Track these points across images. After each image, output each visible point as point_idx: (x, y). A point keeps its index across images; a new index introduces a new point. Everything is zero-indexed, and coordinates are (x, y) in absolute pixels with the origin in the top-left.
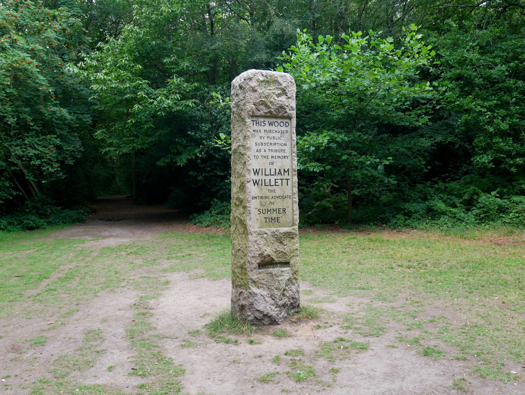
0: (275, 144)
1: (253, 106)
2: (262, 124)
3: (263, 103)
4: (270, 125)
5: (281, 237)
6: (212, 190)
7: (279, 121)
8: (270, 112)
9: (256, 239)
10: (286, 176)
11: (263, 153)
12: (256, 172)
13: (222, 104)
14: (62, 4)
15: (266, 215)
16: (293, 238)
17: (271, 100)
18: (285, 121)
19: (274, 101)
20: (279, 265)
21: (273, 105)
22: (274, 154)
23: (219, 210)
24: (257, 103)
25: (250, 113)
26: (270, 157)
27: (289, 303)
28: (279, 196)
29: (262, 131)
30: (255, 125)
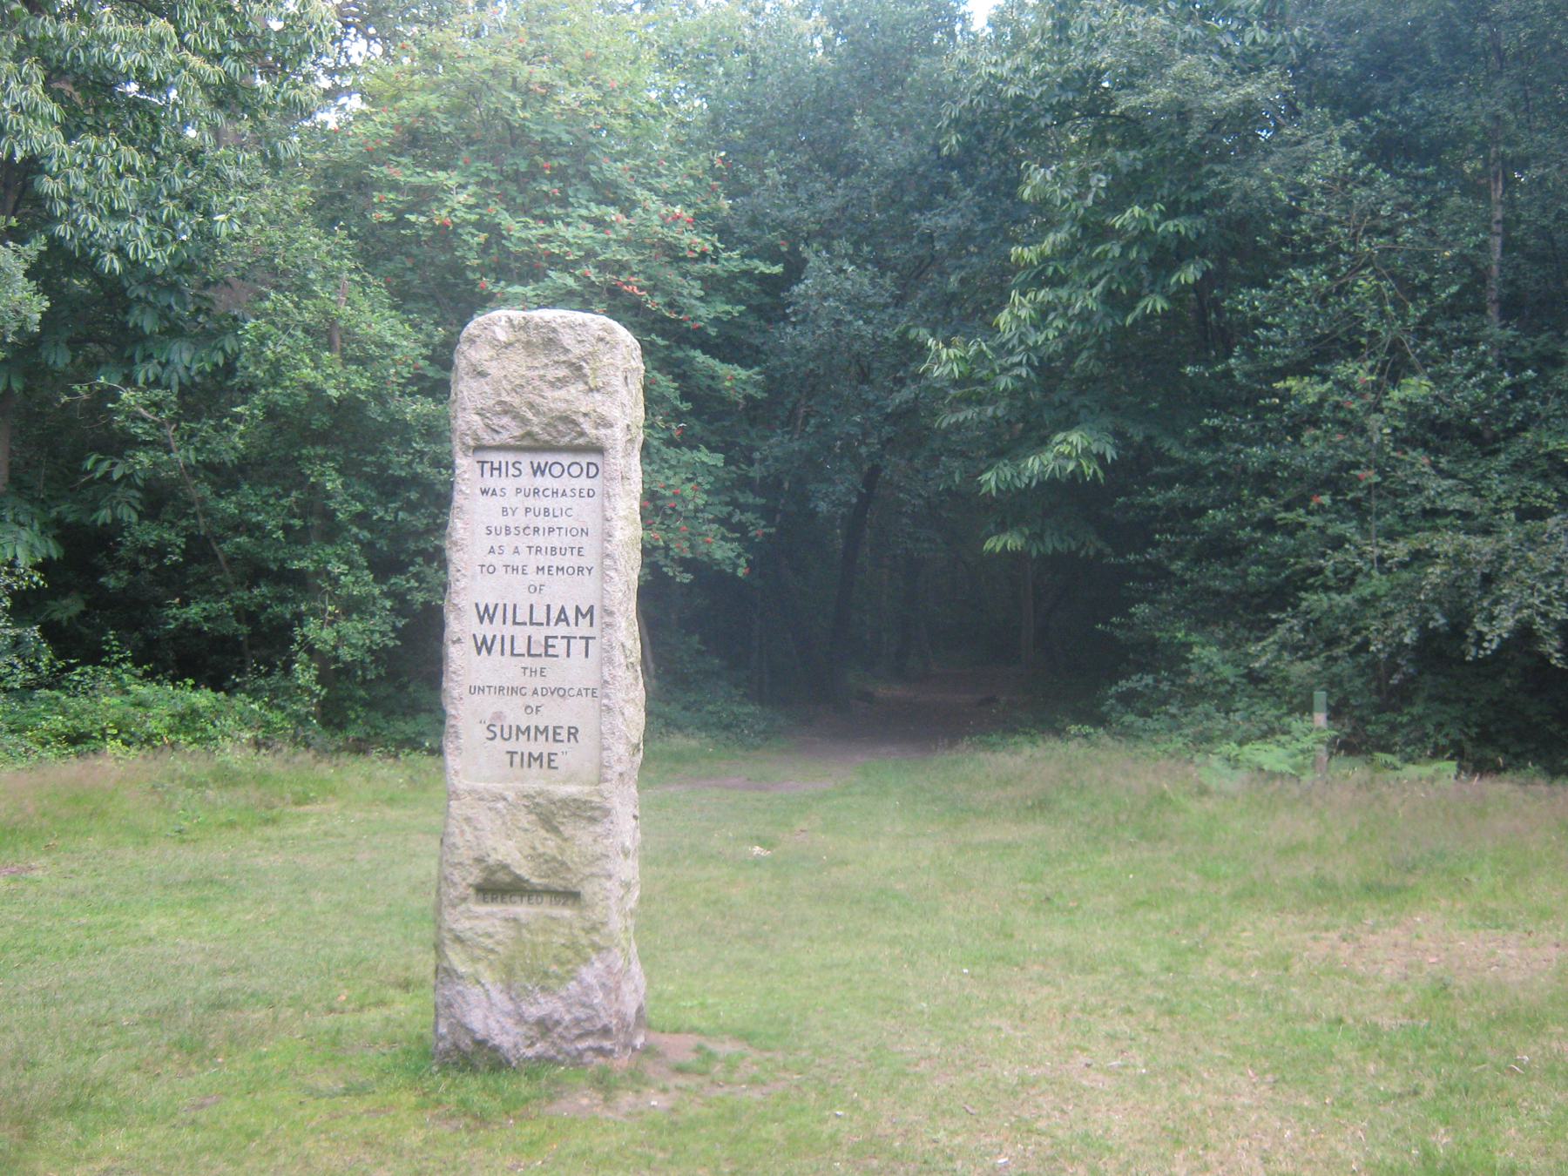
0: (551, 530)
1: (477, 418)
2: (512, 471)
3: (507, 410)
4: (535, 474)
7: (566, 459)
8: (529, 434)
10: (584, 628)
11: (508, 558)
12: (486, 614)
15: (510, 746)
18: (584, 460)
20: (546, 899)
22: (544, 560)
26: (531, 569)
27: (567, 1017)
29: (510, 491)
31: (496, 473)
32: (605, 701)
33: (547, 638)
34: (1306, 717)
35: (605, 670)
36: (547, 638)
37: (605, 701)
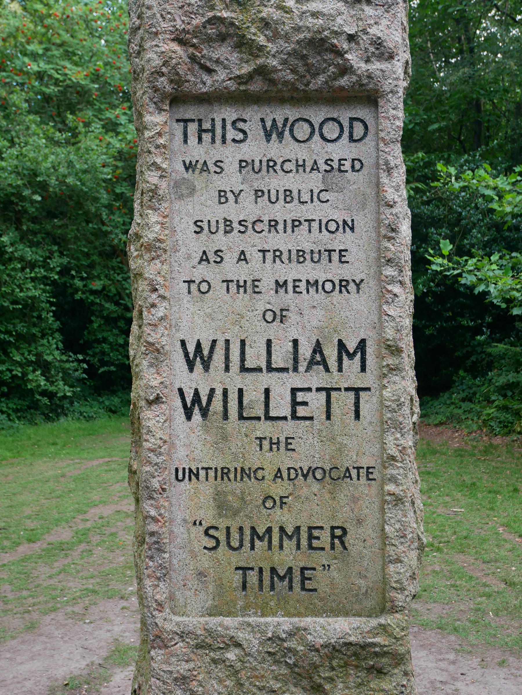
0: (296, 224)
1: (175, 46)
2: (231, 134)
4: (268, 136)
5: (315, 667)
6: (457, 354)
9: (183, 668)
13: (457, 185)
16: (380, 672)
17: (267, 12)
19: (277, 15)
21: (275, 37)
23: (466, 394)
24: (196, 33)
25: (163, 82)
28: (312, 471)
30: (193, 140)
31: (207, 137)
32: (390, 487)
33: (294, 391)
35: (390, 439)
36: (294, 391)
37: (390, 487)
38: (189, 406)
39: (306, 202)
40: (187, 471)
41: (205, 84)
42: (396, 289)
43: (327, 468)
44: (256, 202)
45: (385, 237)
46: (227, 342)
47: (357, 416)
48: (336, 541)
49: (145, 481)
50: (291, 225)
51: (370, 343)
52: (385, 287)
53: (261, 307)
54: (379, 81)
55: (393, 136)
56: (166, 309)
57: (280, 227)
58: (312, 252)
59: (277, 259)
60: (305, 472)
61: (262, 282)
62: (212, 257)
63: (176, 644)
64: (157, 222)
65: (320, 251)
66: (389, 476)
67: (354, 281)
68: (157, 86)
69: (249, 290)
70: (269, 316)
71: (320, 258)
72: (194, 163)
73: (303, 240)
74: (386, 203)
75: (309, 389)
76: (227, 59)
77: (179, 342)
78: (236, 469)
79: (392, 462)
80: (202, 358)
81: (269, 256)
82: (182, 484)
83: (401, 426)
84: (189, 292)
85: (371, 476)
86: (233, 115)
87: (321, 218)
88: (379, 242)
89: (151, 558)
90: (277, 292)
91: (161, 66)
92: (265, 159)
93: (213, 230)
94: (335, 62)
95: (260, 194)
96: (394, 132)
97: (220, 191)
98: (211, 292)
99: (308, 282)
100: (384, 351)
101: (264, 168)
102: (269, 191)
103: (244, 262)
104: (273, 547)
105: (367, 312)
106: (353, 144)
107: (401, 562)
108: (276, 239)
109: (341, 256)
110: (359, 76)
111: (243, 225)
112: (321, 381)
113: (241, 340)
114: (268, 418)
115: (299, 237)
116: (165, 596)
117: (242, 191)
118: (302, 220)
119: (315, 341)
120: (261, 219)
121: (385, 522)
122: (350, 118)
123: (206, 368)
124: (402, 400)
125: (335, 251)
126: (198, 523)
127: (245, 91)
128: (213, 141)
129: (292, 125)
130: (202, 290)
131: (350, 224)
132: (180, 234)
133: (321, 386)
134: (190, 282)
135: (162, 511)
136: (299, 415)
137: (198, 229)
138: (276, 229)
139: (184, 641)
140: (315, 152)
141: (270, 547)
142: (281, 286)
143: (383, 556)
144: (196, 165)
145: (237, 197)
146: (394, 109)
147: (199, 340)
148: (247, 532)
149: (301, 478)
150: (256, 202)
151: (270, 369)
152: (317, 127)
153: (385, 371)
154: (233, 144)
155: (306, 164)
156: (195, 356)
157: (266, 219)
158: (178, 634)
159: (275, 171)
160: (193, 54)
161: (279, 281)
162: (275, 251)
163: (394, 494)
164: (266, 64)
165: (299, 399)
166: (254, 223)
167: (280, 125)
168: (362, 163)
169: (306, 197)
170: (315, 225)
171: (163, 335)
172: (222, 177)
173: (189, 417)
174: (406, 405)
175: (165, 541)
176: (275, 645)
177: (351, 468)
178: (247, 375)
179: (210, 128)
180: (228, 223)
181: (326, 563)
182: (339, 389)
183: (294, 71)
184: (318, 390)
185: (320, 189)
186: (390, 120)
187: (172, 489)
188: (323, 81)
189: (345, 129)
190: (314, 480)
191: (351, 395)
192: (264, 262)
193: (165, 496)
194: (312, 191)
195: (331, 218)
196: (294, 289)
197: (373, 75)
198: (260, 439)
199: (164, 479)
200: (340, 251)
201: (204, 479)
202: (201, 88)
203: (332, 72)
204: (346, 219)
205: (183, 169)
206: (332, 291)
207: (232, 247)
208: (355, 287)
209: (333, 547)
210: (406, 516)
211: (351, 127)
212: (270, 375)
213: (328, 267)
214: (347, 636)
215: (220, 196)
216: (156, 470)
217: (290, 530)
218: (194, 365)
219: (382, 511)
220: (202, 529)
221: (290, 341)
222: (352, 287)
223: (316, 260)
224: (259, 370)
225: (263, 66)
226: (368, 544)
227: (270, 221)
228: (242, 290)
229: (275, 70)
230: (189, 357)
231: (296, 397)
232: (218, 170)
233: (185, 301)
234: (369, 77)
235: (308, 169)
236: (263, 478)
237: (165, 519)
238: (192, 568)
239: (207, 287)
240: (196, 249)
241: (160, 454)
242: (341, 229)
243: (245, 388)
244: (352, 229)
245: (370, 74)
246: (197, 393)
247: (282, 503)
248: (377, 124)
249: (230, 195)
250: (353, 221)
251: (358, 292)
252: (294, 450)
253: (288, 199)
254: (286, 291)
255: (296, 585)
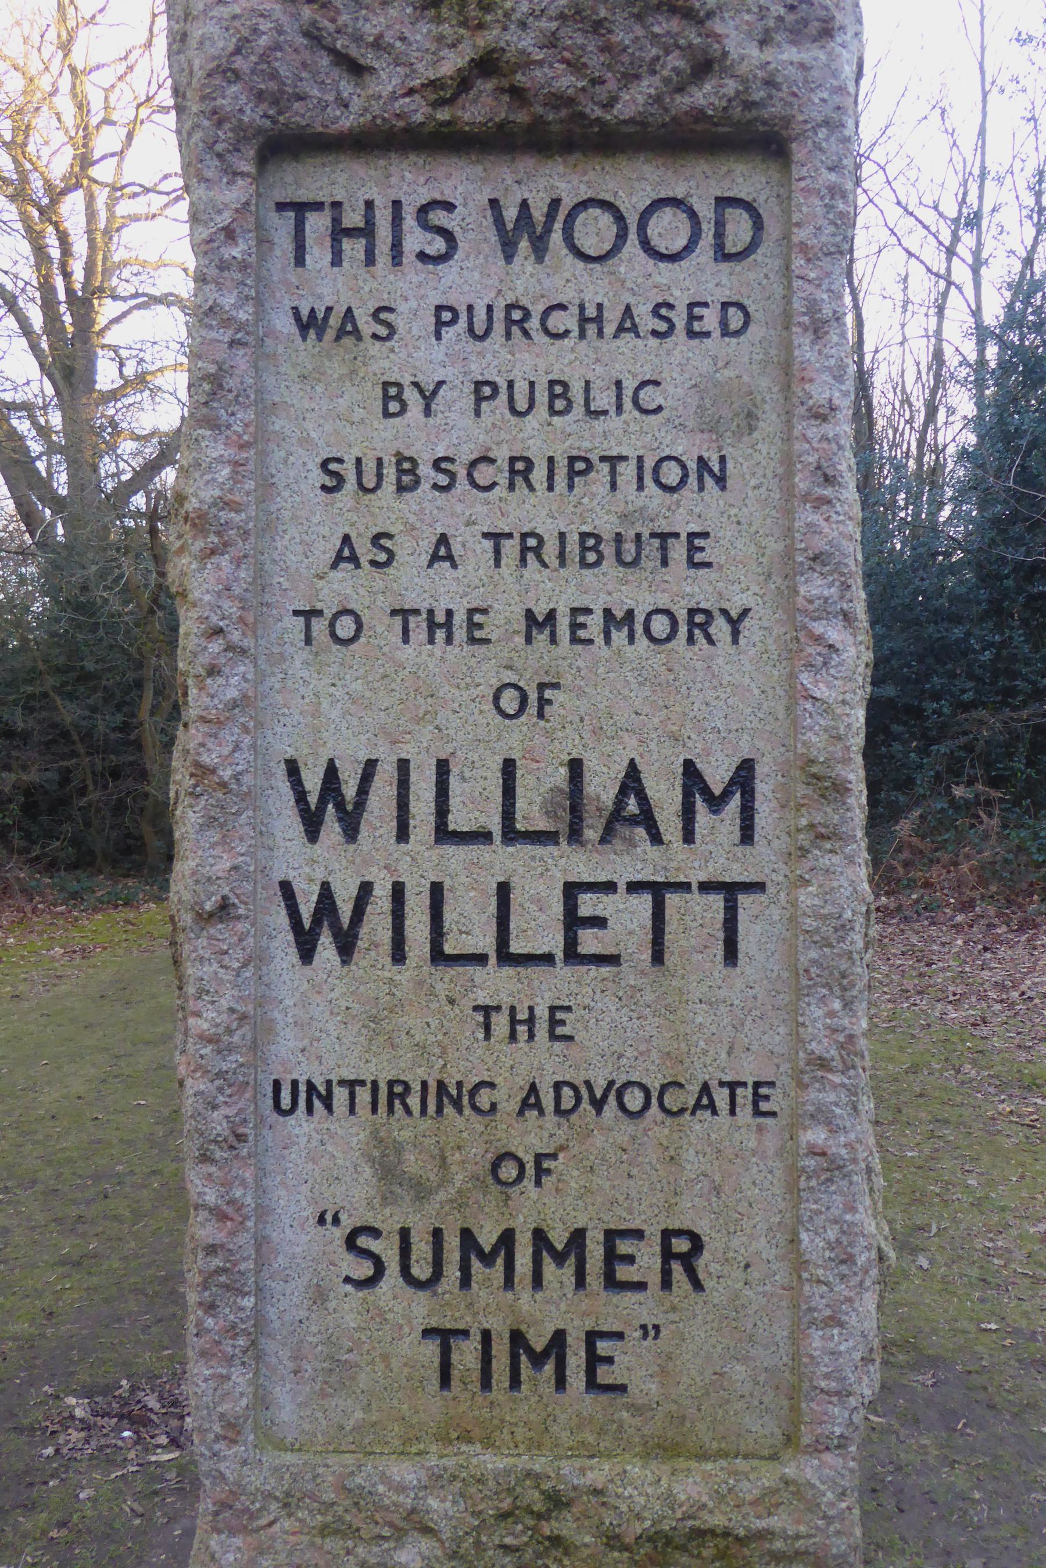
2: (415, 239)
14: (16, 147)
30: (318, 255)
32: (816, 1135)
33: (572, 890)
34: (150, 778)
36: (572, 890)
38: (307, 926)
39: (605, 413)
40: (303, 1088)
41: (346, 106)
42: (835, 633)
43: (654, 1085)
44: (478, 413)
45: (806, 498)
46: (403, 766)
47: (731, 954)
48: (677, 1267)
49: (192, 1117)
50: (565, 470)
51: (766, 770)
52: (804, 627)
53: (490, 677)
54: (795, 95)
55: (830, 239)
56: (246, 680)
57: (539, 475)
58: (619, 538)
59: (530, 557)
60: (599, 1094)
61: (492, 614)
62: (365, 551)
63: (271, 1524)
64: (220, 460)
65: (638, 536)
66: (811, 1108)
67: (724, 612)
68: (222, 106)
69: (460, 634)
70: (509, 701)
71: (638, 554)
72: (320, 315)
73: (598, 509)
74: (810, 410)
75: (609, 887)
76: (403, 39)
77: (283, 766)
78: (424, 1084)
79: (820, 1073)
80: (340, 806)
81: (511, 548)
82: (291, 1120)
83: (845, 982)
84: (308, 641)
85: (764, 1106)
86: (421, 190)
87: (641, 453)
88: (789, 513)
89: (210, 1308)
90: (529, 640)
91: (233, 54)
92: (500, 304)
93: (370, 482)
94: (682, 42)
95: (487, 391)
96: (831, 229)
97: (386, 385)
98: (363, 640)
99: (608, 613)
100: (801, 790)
101: (499, 327)
102: (511, 384)
103: (447, 564)
104: (516, 1280)
105: (756, 692)
106: (725, 266)
107: (841, 1325)
108: (527, 506)
109: (692, 549)
110: (744, 80)
111: (445, 471)
112: (639, 866)
113: (439, 761)
114: (506, 957)
115: (586, 500)
116: (244, 1402)
117: (440, 384)
118: (594, 458)
119: (626, 763)
120: (491, 455)
121: (799, 1221)
122: (717, 199)
123: (351, 831)
124: (848, 914)
125: (676, 535)
126: (329, 1217)
127: (449, 123)
128: (370, 260)
129: (571, 218)
130: (341, 633)
131: (716, 469)
132: (286, 494)
133: (639, 877)
134: (310, 614)
135: (238, 1193)
136: (582, 950)
137: (329, 482)
138: (527, 480)
139: (290, 1515)
140: (629, 284)
141: (509, 1282)
142: (541, 626)
143: (796, 1306)
144: (326, 318)
145: (428, 398)
146: (831, 169)
147: (331, 762)
148: (452, 1243)
149: (589, 1107)
150: (478, 413)
151: (511, 834)
152: (633, 236)
153: (804, 839)
154: (419, 265)
155: (606, 314)
156: (323, 800)
157: (502, 455)
158: (276, 1498)
159: (526, 333)
160: (314, 23)
161: (536, 610)
162: (524, 536)
163: (824, 1154)
164: (502, 44)
165: (584, 911)
166: (473, 464)
167: (538, 214)
168: (747, 314)
169: (603, 399)
170: (627, 471)
171: (237, 748)
172: (392, 350)
173: (307, 954)
174: (857, 928)
175: (243, 1266)
176: (520, 1527)
177: (714, 1084)
178: (450, 849)
179: (362, 225)
180: (406, 466)
181: (650, 1321)
182: (685, 887)
183: (575, 66)
184: (634, 887)
185: (640, 378)
186: (822, 198)
187: (265, 1132)
188: (650, 96)
189: (704, 226)
190: (620, 1114)
191: (717, 901)
192: (497, 563)
193: (244, 1152)
194: (618, 384)
195: (667, 452)
196: (573, 633)
197: (779, 80)
198: (487, 1011)
199: (241, 1111)
200: (691, 536)
201: (345, 1110)
202: (337, 119)
203: (674, 69)
204: (706, 455)
205: (294, 330)
206: (669, 639)
207: (418, 525)
208: (726, 628)
209: (666, 1283)
210: (853, 1210)
211: (720, 225)
212: (510, 849)
213: (658, 578)
214: (701, 1514)
215: (386, 398)
216: (220, 1090)
217: (559, 1239)
218: (321, 823)
219: (793, 1190)
220: (339, 1235)
221: (561, 765)
222: (720, 628)
223: (629, 559)
224: (483, 836)
225: (494, 51)
226: (755, 1274)
227: (513, 460)
228: (440, 635)
229: (526, 63)
230: (307, 803)
231: (575, 907)
232: (383, 332)
233: (298, 663)
234: (770, 83)
235: (609, 329)
236: (494, 1106)
237: (244, 1211)
238: (314, 1329)
239: (353, 627)
240: (325, 531)
241: (230, 1049)
242: (693, 479)
243: (447, 883)
244: (721, 481)
245: (772, 74)
246: (326, 893)
247: (541, 1173)
248: (787, 212)
249: (411, 396)
250: (722, 459)
251: (735, 641)
252: (570, 1038)
253: (560, 404)
254: (553, 640)
255: (576, 1379)
